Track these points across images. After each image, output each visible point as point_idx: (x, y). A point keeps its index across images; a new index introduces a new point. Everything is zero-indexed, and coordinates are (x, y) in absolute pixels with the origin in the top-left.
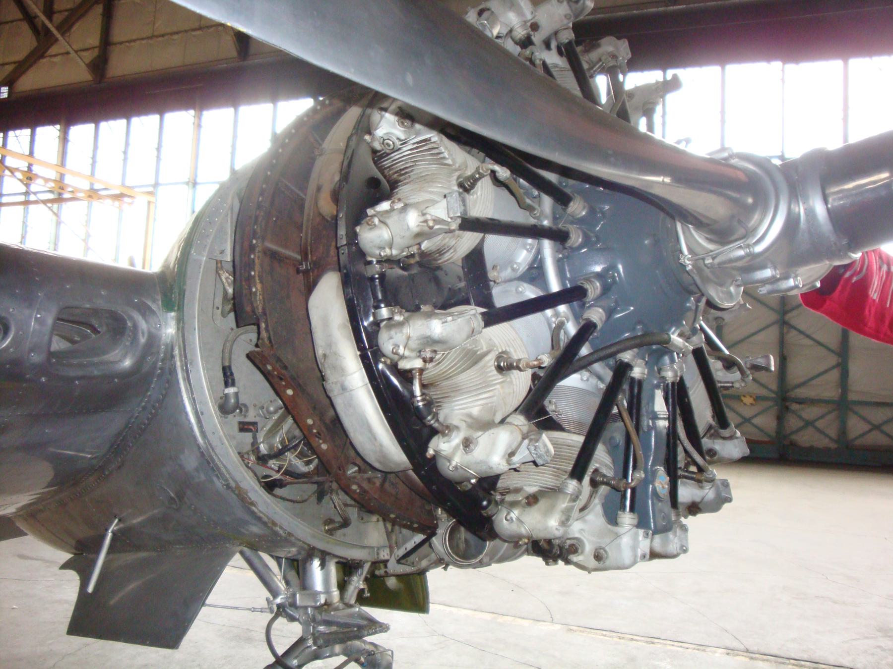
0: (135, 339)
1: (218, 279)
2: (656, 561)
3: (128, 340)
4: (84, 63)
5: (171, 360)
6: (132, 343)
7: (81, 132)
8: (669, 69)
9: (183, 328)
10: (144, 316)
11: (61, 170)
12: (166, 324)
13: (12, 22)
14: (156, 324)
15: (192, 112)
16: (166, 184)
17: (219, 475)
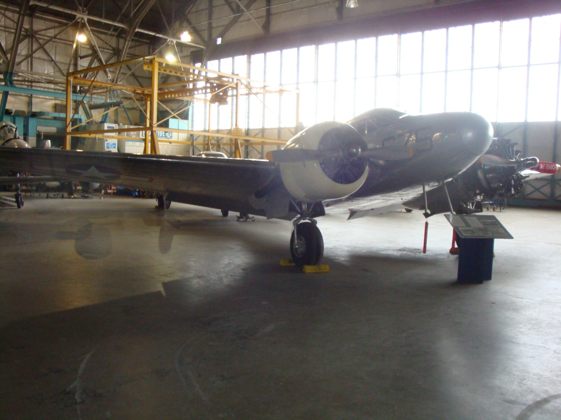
2: (356, 222)
7: (258, 58)
8: (236, 56)
11: (249, 80)
13: (220, 5)
15: (246, 56)
16: (524, 66)
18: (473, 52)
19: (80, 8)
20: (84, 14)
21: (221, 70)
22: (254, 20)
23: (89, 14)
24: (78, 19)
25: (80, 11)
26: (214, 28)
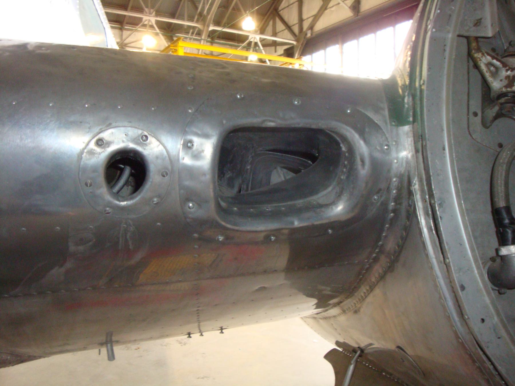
0: (352, 170)
1: (474, 72)
3: (343, 171)
4: (347, 6)
5: (409, 198)
6: (348, 177)
9: (424, 147)
10: (362, 133)
12: (397, 143)
14: (381, 146)
17: (490, 380)
19: (146, 10)
20: (150, 15)
23: (157, 15)
24: (144, 22)
25: (146, 13)
26: (304, 20)
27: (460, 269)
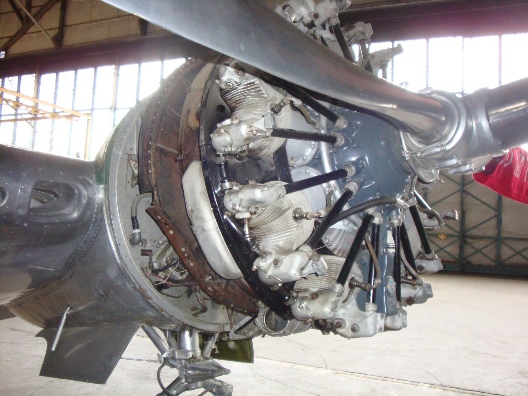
0: (80, 200)
1: (129, 165)
3: (75, 201)
4: (50, 37)
5: (101, 213)
6: (78, 203)
7: (48, 78)
9: (108, 194)
10: (85, 187)
12: (98, 192)
13: (7, 13)
14: (92, 192)
15: (113, 66)
16: (98, 109)
17: (130, 281)
18: (427, 72)
21: (21, 91)
22: (43, 32)
27: (119, 238)
